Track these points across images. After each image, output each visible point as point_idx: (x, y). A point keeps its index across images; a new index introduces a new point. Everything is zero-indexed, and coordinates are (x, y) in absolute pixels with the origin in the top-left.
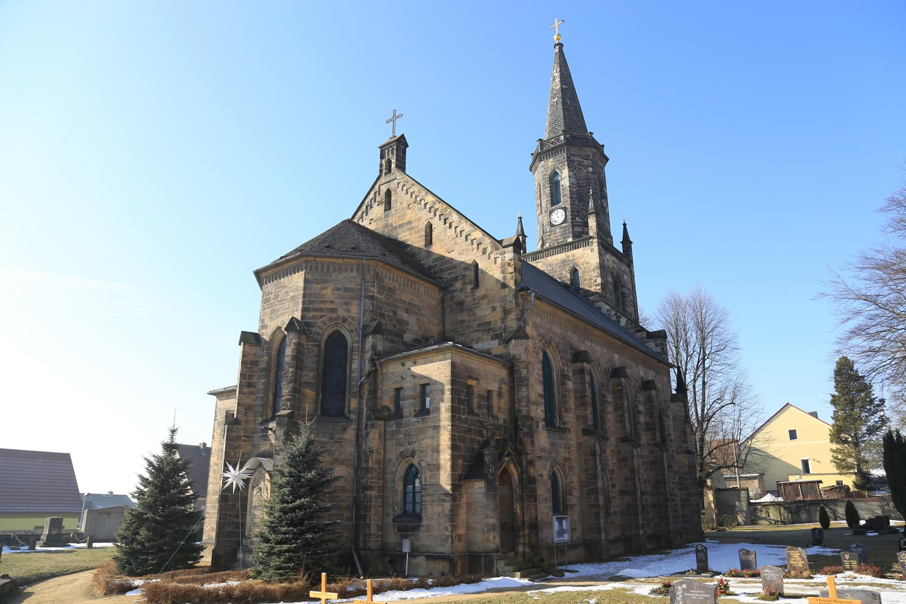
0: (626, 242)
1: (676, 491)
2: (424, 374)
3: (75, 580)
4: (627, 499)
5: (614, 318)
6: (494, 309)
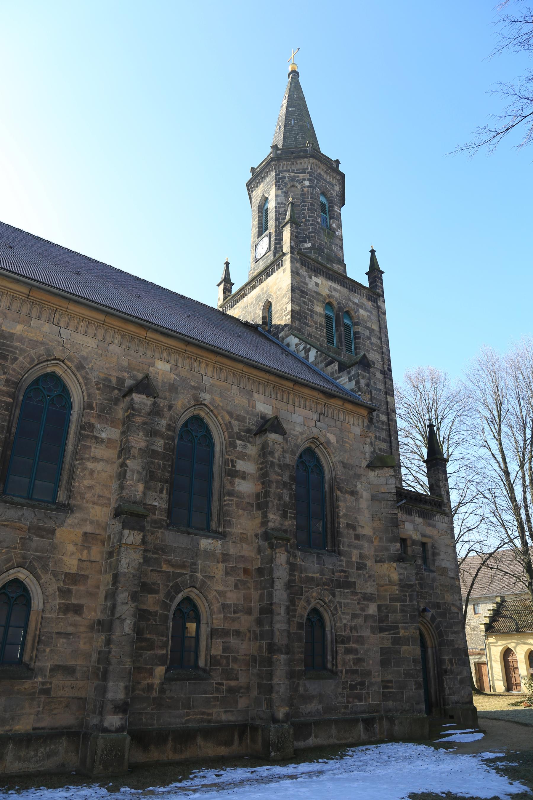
0: (375, 272)
1: (367, 633)
3: (513, 705)
4: (100, 639)
5: (303, 354)
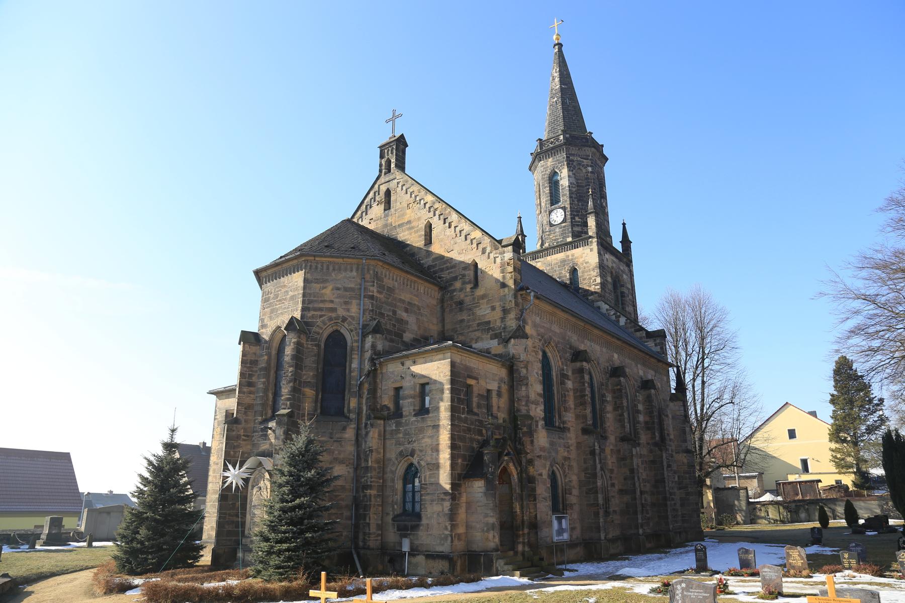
0: (626, 242)
1: (675, 490)
2: (423, 373)
4: (627, 498)
5: (614, 318)
6: (493, 308)
